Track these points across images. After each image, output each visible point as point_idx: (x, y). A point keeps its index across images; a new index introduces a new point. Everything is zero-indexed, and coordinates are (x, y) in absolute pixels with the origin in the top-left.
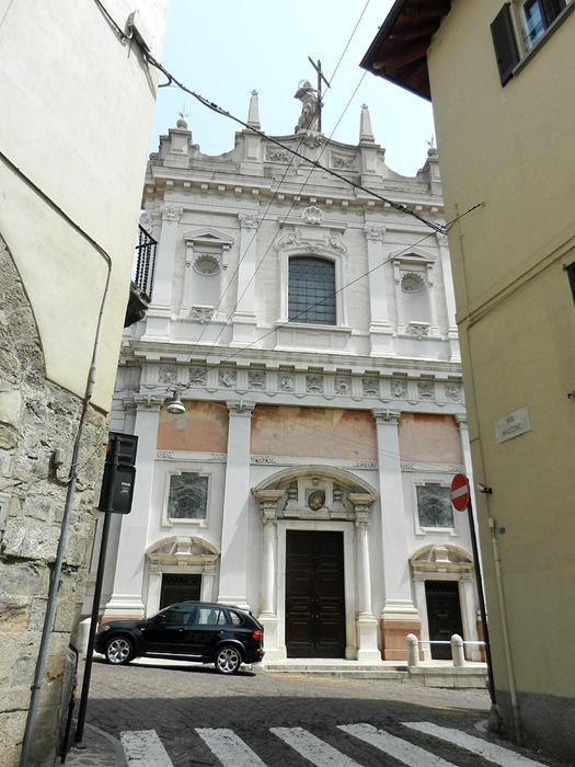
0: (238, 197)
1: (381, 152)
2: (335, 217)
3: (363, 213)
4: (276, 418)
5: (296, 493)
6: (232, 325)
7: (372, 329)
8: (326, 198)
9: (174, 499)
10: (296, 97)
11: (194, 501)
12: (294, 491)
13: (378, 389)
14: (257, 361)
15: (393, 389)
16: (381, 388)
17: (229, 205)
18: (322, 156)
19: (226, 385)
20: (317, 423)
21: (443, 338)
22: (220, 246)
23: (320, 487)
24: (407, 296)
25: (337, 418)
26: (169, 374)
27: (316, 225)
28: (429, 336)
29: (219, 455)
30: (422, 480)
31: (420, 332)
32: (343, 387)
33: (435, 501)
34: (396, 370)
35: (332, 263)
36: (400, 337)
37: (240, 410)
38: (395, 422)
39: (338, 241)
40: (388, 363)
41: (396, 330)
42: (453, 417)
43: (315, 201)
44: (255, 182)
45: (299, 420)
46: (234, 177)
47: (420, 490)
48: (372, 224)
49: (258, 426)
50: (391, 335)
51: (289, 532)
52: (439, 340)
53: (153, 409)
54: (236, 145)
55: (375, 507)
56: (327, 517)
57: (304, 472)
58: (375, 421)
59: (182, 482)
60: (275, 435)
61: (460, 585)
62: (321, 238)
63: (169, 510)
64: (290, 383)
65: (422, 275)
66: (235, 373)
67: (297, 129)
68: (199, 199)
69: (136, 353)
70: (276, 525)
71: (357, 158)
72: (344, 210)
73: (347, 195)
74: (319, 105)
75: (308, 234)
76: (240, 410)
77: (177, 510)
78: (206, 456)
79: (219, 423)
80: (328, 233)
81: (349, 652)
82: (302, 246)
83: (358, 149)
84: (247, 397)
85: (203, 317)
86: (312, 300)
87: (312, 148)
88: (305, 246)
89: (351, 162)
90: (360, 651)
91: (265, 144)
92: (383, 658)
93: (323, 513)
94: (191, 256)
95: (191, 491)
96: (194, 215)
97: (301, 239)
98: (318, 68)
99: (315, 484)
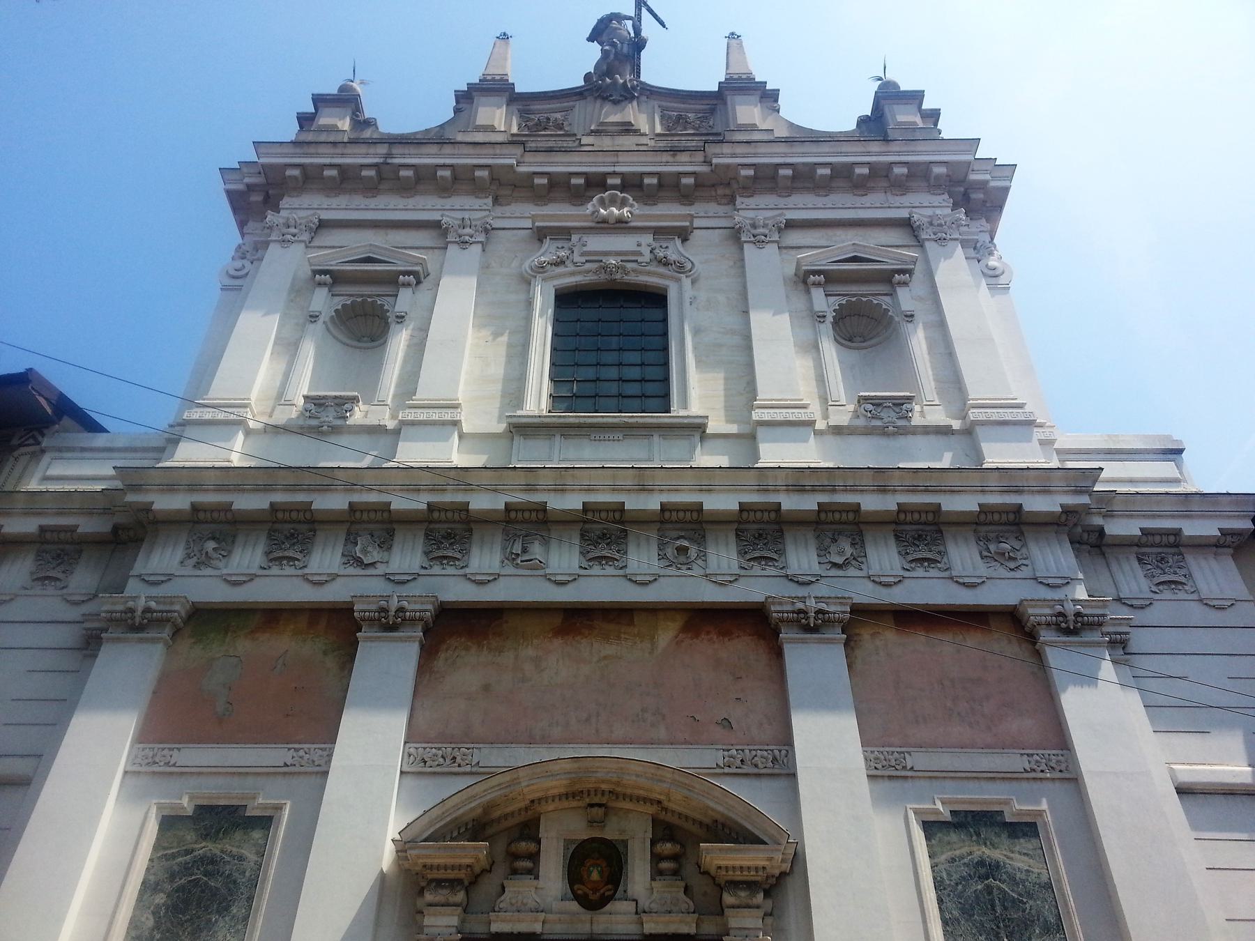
2: (669, 212)
3: (731, 200)
5: (535, 857)
6: (397, 432)
7: (757, 415)
8: (642, 175)
12: (524, 846)
14: (448, 498)
15: (823, 551)
17: (426, 207)
18: (642, 118)
20: (610, 649)
21: (956, 425)
23: (610, 833)
24: (853, 356)
25: (666, 634)
26: (211, 545)
27: (620, 226)
31: (888, 415)
32: (682, 550)
33: (988, 869)
34: (824, 498)
35: (657, 299)
36: (837, 430)
39: (674, 249)
40: (801, 479)
41: (826, 417)
43: (617, 181)
44: (479, 156)
45: (558, 642)
46: (433, 149)
48: (751, 214)
49: (440, 662)
50: (811, 423)
52: (943, 431)
57: (557, 785)
58: (777, 633)
60: (486, 688)
62: (634, 248)
64: (537, 550)
65: (885, 301)
66: (861, 533)
68: (359, 201)
75: (597, 243)
80: (647, 239)
82: (588, 266)
84: (415, 589)
85: (329, 417)
87: (615, 103)
88: (595, 265)
94: (322, 301)
95: (213, 861)
96: (651, 399)
97: (583, 254)
99: (591, 823)
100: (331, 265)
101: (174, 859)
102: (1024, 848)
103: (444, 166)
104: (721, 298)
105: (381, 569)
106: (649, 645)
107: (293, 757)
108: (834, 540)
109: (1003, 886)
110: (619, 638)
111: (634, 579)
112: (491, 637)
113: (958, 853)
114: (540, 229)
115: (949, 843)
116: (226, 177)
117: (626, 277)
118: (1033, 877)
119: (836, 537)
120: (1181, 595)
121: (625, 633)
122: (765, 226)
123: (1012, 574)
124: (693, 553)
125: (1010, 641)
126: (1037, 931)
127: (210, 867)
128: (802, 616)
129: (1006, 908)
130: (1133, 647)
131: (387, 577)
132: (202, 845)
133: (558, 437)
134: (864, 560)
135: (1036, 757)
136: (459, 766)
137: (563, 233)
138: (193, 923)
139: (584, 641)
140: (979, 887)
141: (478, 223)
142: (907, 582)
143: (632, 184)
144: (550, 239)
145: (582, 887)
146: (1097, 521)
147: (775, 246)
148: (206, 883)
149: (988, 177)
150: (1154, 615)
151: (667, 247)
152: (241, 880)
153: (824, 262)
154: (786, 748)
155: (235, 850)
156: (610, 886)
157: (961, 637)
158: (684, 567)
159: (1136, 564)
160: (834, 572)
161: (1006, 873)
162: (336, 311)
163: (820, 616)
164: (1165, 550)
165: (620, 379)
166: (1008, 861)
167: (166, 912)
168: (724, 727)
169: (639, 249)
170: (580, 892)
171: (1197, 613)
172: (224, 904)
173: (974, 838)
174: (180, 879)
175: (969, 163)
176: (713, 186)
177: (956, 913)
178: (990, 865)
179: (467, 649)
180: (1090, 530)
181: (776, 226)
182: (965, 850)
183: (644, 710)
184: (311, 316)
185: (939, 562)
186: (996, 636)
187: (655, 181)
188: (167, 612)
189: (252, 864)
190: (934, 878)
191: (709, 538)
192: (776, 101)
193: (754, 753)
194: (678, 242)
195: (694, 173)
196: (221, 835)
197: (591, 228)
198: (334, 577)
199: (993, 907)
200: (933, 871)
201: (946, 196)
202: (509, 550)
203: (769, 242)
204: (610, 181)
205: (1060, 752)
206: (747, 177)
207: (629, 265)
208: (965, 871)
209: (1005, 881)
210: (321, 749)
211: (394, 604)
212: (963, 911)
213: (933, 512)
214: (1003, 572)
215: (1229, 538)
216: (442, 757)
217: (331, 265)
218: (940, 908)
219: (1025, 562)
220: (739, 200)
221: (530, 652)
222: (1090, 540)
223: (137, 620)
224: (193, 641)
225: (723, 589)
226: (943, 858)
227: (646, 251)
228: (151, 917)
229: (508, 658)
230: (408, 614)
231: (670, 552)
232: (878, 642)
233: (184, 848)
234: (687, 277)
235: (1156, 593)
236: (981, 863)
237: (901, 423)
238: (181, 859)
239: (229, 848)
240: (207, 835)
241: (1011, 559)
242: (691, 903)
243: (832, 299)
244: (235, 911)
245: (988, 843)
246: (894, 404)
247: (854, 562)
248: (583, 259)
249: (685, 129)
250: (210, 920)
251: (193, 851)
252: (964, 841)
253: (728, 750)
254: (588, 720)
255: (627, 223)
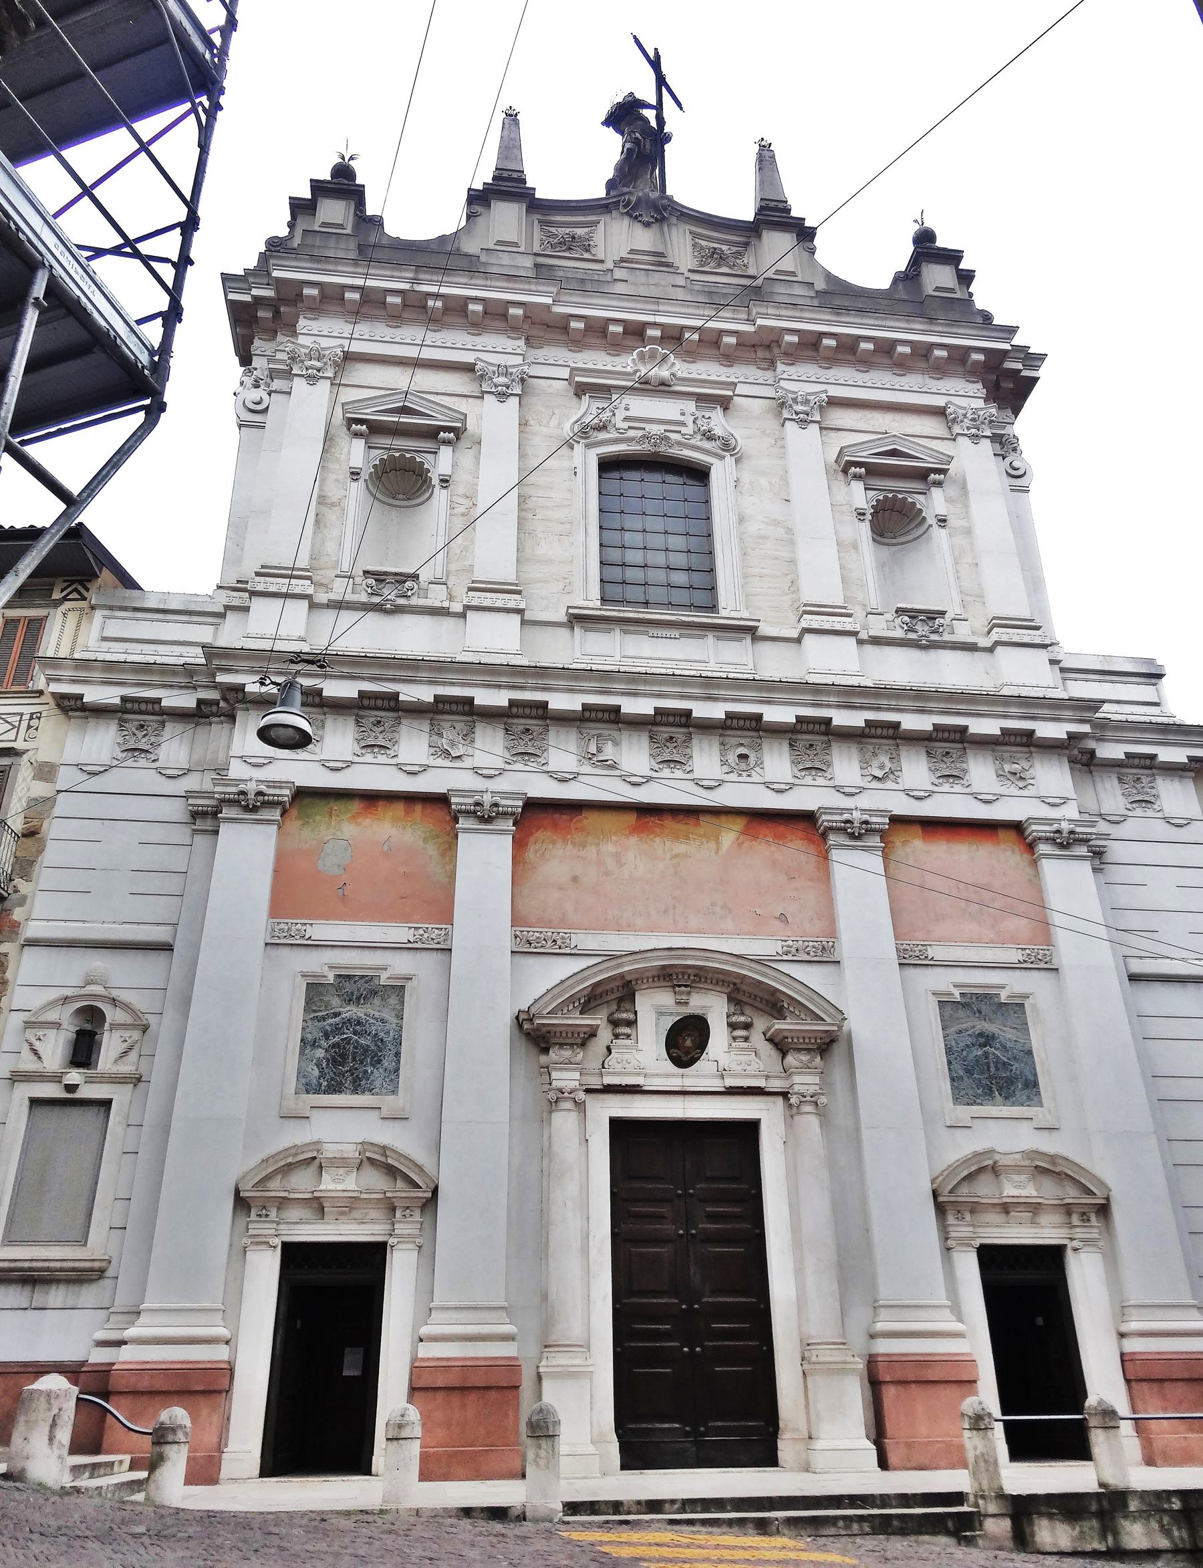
0: (475, 325)
1: (805, 234)
3: (772, 365)
4: (577, 837)
5: (632, 1023)
8: (683, 328)
9: (314, 1044)
10: (608, 122)
11: (366, 1050)
13: (829, 764)
15: (865, 764)
16: (696, 754)
19: (447, 753)
20: (680, 848)
22: (432, 434)
27: (662, 389)
28: (947, 637)
29: (434, 931)
30: (946, 981)
31: (923, 629)
33: (987, 1039)
35: (699, 474)
37: (486, 816)
38: (875, 841)
39: (717, 421)
42: (1017, 827)
45: (633, 840)
47: (948, 1011)
49: (531, 854)
51: (619, 1127)
53: (265, 814)
54: (469, 217)
55: (838, 1050)
56: (716, 1085)
59: (335, 1002)
60: (575, 879)
61: (1070, 1257)
63: (301, 1073)
64: (609, 752)
67: (611, 185)
68: (382, 330)
69: (221, 678)
70: (580, 1106)
71: (751, 250)
72: (728, 358)
73: (734, 320)
74: (660, 138)
75: (642, 406)
76: (486, 816)
77: (322, 1075)
78: (399, 933)
79: (432, 850)
80: (690, 406)
81: (786, 1449)
82: (631, 433)
83: (750, 231)
84: (503, 784)
86: (659, 558)
88: (640, 433)
89: (739, 255)
90: (819, 1444)
91: (536, 217)
92: (883, 1464)
93: (701, 1075)
94: (859, 496)
95: (359, 1023)
97: (626, 419)
98: (655, 63)
100: (367, 414)
101: (324, 1021)
102: (1014, 1023)
103: (476, 300)
104: (764, 482)
105: (468, 763)
106: (714, 846)
107: (415, 935)
108: (875, 754)
109: (996, 1052)
110: (688, 838)
111: (700, 783)
112: (573, 831)
113: (964, 1026)
114: (579, 384)
115: (957, 1019)
116: (228, 284)
117: (670, 450)
118: (1018, 1046)
119: (877, 751)
120: (1150, 813)
121: (692, 834)
122: (807, 402)
123: (1021, 793)
124: (752, 759)
125: (1013, 852)
126: (1020, 1087)
127: (358, 1028)
128: (848, 825)
129: (997, 1069)
130: (1108, 858)
131: (475, 770)
132: (348, 1008)
133: (618, 631)
134: (899, 773)
135: (1028, 951)
136: (560, 948)
137: (603, 391)
138: (352, 1074)
139: (658, 840)
140: (979, 1053)
141: (514, 370)
142: (936, 797)
143: (673, 337)
144: (590, 397)
145: (676, 1051)
146: (1092, 744)
147: (817, 426)
148: (357, 1041)
149: (1020, 366)
150: (1128, 829)
151: (709, 418)
152: (387, 1039)
153: (864, 454)
154: (833, 940)
155: (377, 1014)
156: (698, 1051)
157: (975, 846)
158: (744, 774)
159: (1116, 781)
160: (875, 784)
161: (1000, 1042)
162: (375, 466)
163: (864, 826)
164: (1141, 771)
165: (668, 567)
166: (1001, 1033)
167: (328, 1064)
168: (782, 921)
169: (682, 418)
170: (674, 1054)
171: (1161, 830)
172: (376, 1059)
173: (977, 1015)
174: (334, 1037)
175: (1005, 352)
176: (753, 346)
177: (961, 1073)
178: (988, 1037)
179: (554, 843)
180: (1083, 752)
181: (818, 403)
182: (969, 1024)
183: (714, 904)
184: (352, 473)
185: (963, 779)
186: (1003, 846)
187: (696, 337)
188: (279, 796)
189: (394, 1026)
190: (946, 1045)
191: (765, 746)
192: (812, 240)
193: (806, 943)
194: (719, 410)
195: (736, 332)
196: (362, 1001)
197: (631, 388)
198: (426, 768)
199: (989, 1068)
200: (945, 1040)
201: (980, 386)
202: (584, 749)
203: (812, 421)
204: (651, 332)
205: (1046, 947)
206: (791, 344)
207: (673, 436)
208: (969, 1041)
209: (998, 1049)
210: (437, 929)
211: (487, 799)
212: (967, 1071)
213: (960, 732)
214: (1013, 790)
215: (1193, 764)
216: (544, 939)
217: (367, 414)
218: (949, 1068)
219: (1031, 782)
220: (780, 367)
221: (611, 848)
222: (1083, 760)
223: (251, 802)
224: (301, 822)
225: (779, 796)
226: (952, 1030)
227: (689, 420)
228: (315, 1068)
229: (591, 852)
230: (501, 809)
231: (732, 758)
232: (908, 850)
233: (332, 1011)
234: (731, 455)
235: (1129, 810)
236: (981, 1034)
237: (934, 637)
238: (330, 1020)
239: (372, 1012)
240: (350, 1001)
241: (1021, 778)
242: (761, 1063)
243: (871, 493)
244: (386, 1064)
245: (987, 1019)
246: (928, 618)
247: (891, 776)
248: (626, 425)
249: (719, 265)
250: (367, 1071)
251: (340, 1014)
252: (969, 1017)
253: (786, 941)
254: (665, 912)
255: (669, 386)
